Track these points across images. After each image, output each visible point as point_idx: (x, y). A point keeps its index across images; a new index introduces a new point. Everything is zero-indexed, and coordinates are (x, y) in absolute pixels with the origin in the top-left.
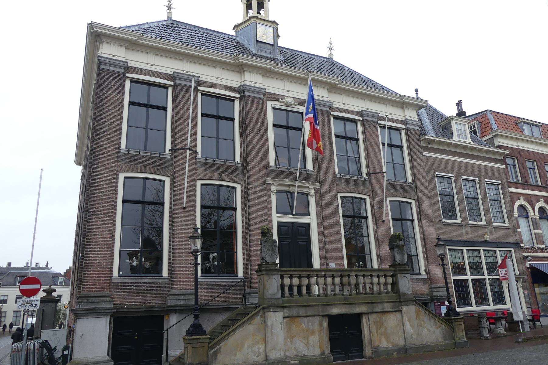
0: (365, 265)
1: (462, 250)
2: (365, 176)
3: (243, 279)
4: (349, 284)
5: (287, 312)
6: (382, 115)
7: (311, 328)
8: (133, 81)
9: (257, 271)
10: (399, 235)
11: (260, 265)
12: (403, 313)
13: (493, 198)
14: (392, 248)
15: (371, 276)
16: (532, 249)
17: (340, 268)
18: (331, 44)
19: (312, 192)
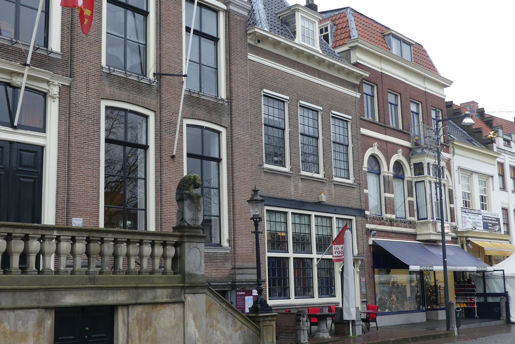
0: (135, 225)
1: (286, 213)
10: (195, 178)
13: (338, 141)
14: (180, 199)
15: (141, 243)
16: (380, 220)
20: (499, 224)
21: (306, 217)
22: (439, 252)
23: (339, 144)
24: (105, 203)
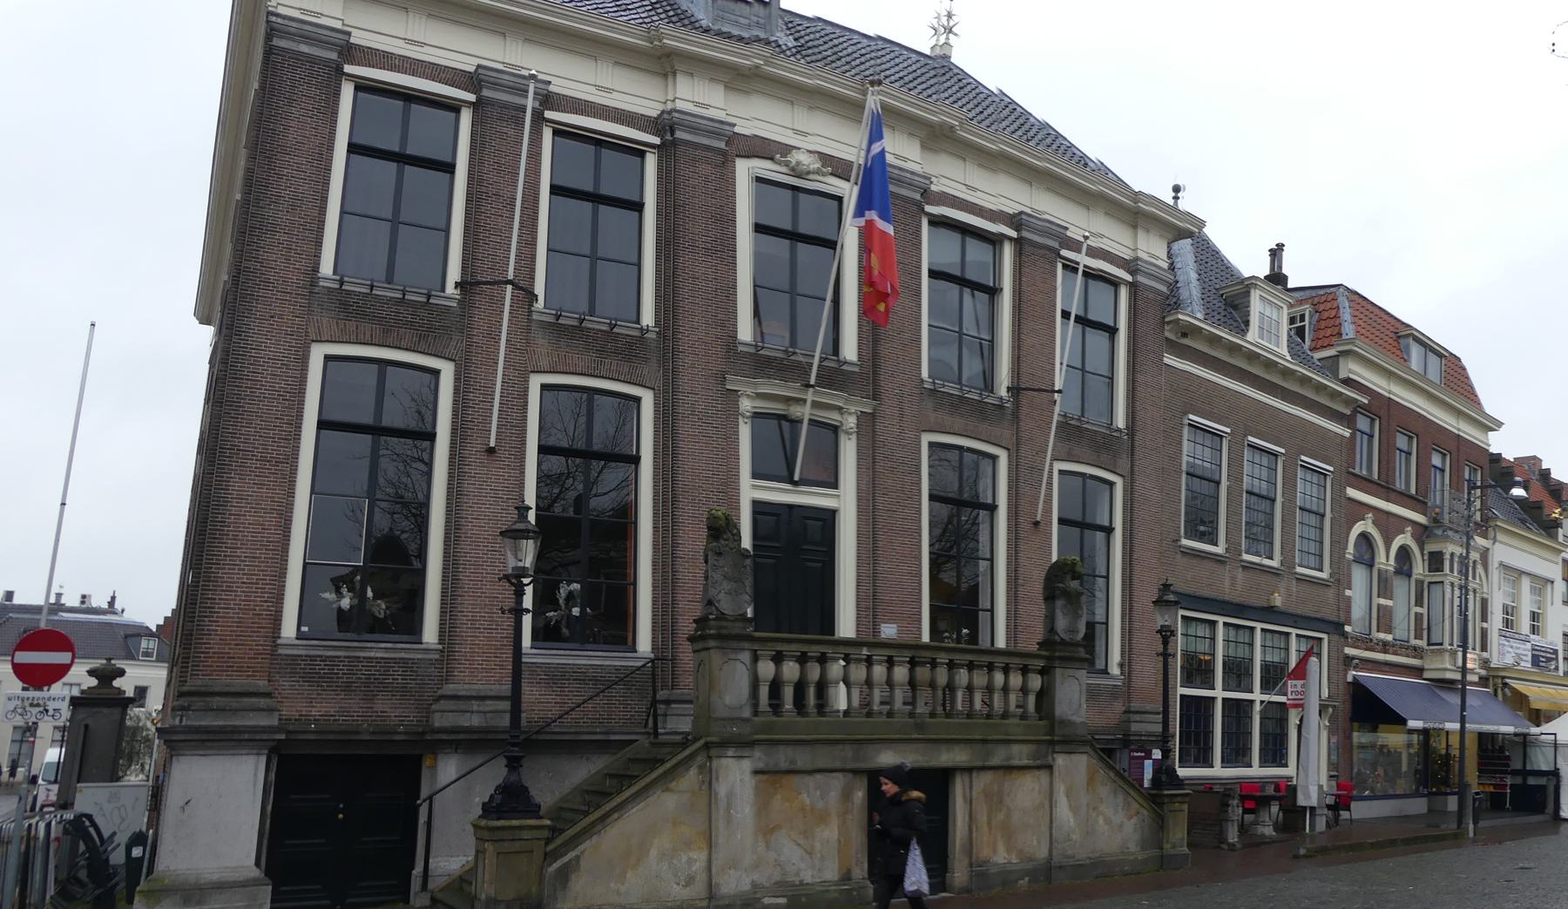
0: (973, 637)
1: (1214, 623)
2: (1003, 392)
3: (652, 661)
4: (932, 685)
5: (758, 758)
7: (820, 805)
8: (362, 87)
9: (692, 639)
10: (1074, 564)
11: (701, 622)
12: (1056, 773)
13: (1308, 506)
14: (1050, 597)
15: (991, 667)
16: (1366, 642)
17: (908, 638)
18: (949, 16)
19: (851, 422)
20: (1557, 659)
21: (1247, 632)
22: (1455, 700)
23: (1310, 511)
24: (932, 598)
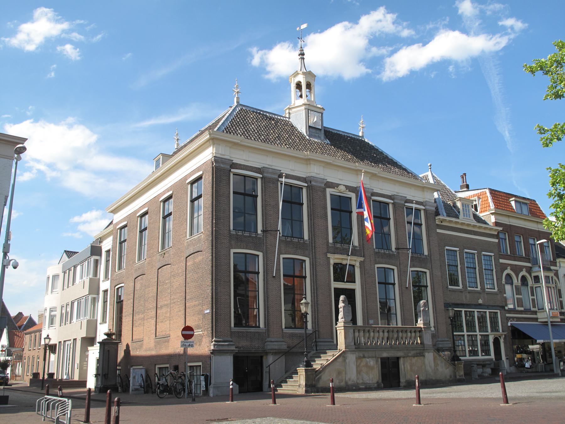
2: (393, 249)
6: (409, 197)
